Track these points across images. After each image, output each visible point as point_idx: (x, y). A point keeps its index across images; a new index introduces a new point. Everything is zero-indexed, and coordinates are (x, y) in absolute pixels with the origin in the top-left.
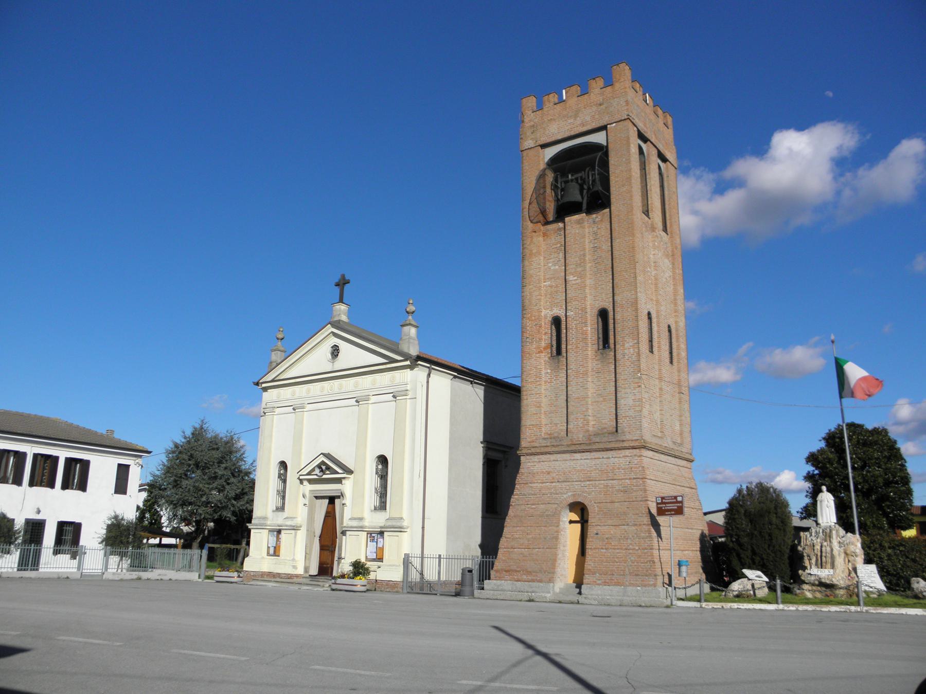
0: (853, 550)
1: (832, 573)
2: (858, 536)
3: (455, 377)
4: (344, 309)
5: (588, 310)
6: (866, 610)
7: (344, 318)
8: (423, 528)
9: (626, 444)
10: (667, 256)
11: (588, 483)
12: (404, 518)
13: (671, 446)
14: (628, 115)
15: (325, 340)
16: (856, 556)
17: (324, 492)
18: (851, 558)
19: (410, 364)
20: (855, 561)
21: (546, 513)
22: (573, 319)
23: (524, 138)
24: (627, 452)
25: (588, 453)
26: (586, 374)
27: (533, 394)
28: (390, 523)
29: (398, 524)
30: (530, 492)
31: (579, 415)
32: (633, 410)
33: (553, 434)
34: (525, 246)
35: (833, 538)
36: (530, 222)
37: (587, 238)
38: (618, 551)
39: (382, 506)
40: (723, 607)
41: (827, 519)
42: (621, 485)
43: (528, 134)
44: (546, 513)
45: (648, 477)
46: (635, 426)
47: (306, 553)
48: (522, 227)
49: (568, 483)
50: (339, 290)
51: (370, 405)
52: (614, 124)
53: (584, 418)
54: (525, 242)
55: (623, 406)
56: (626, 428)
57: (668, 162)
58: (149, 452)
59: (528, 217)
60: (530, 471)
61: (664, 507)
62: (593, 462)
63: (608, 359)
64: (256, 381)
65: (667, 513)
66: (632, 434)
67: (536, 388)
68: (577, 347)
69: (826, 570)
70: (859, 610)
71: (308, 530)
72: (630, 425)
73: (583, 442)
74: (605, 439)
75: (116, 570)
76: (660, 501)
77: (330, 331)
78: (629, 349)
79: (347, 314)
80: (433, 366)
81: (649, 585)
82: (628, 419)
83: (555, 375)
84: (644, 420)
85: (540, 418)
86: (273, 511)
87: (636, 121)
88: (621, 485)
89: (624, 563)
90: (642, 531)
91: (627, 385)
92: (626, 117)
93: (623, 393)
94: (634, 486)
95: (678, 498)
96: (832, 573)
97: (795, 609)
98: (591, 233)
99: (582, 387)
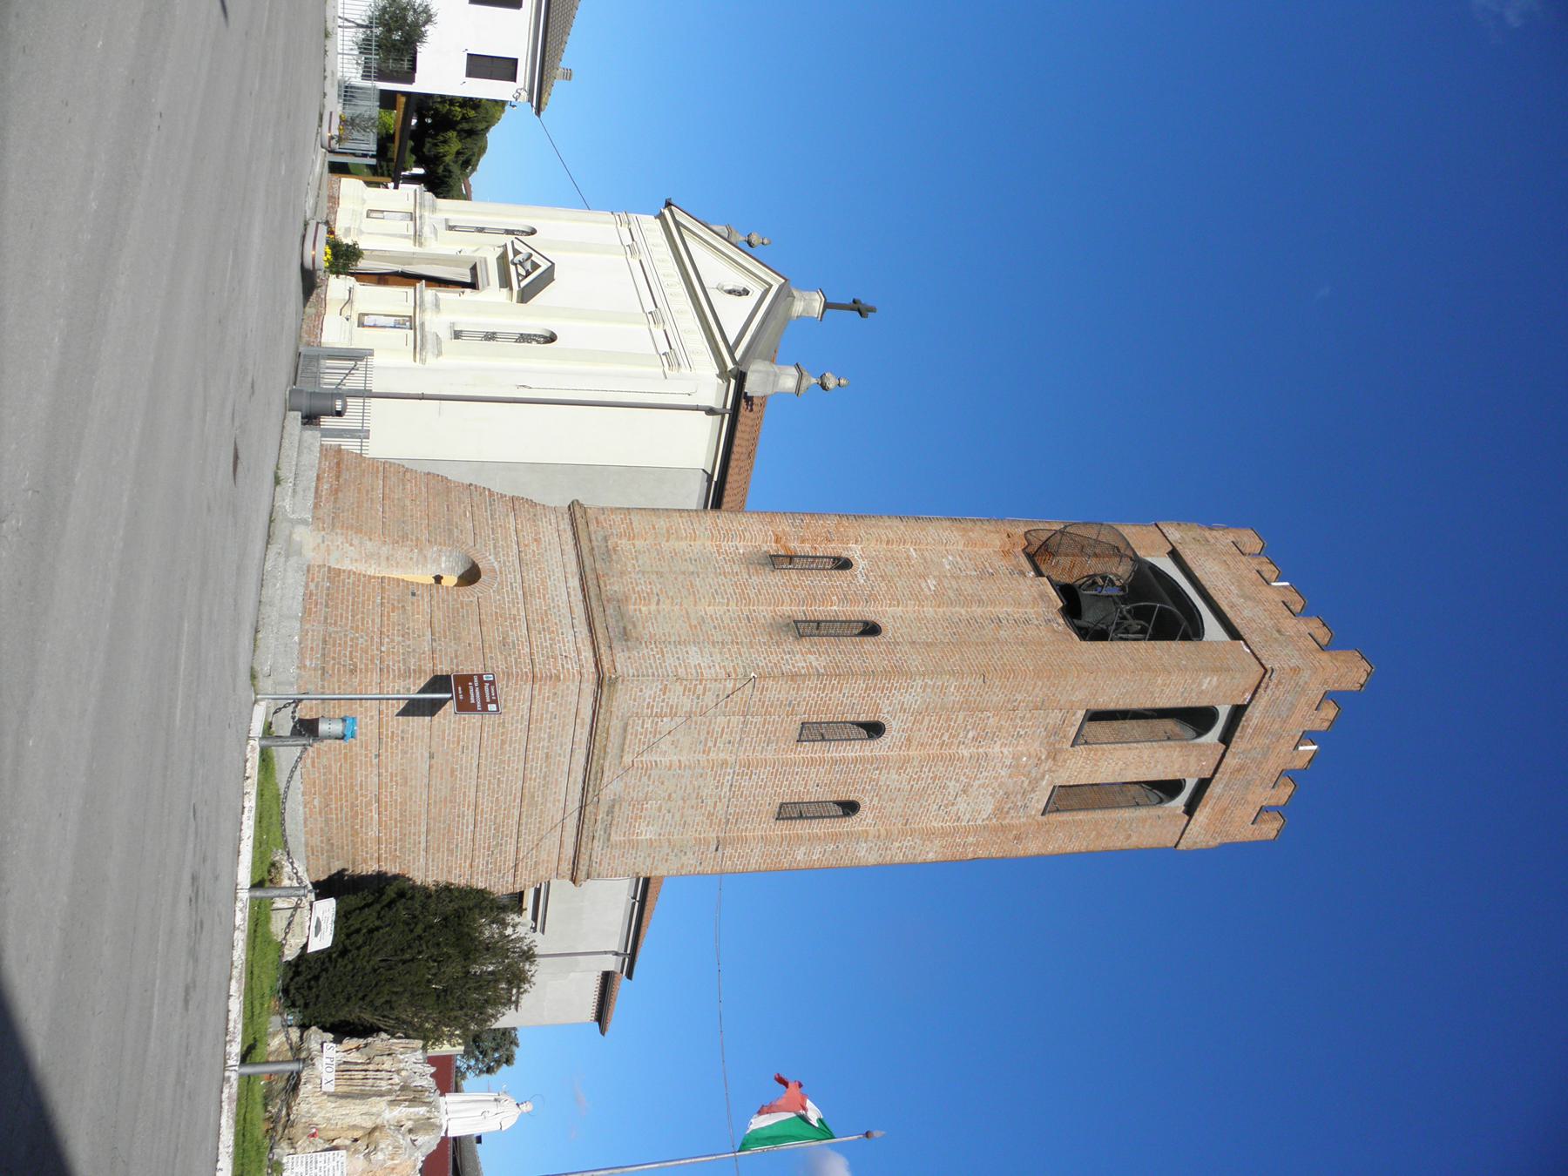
0: (382, 1146)
3: (710, 477)
4: (814, 307)
6: (229, 1077)
7: (798, 308)
8: (422, 397)
9: (603, 649)
11: (520, 593)
12: (440, 358)
13: (607, 794)
14: (1273, 670)
15: (759, 281)
16: (367, 1156)
17: (484, 272)
18: (361, 1145)
19: (729, 369)
20: (356, 1151)
21: (455, 530)
22: (851, 583)
23: (1181, 528)
24: (587, 654)
25: (581, 598)
27: (692, 524)
28: (430, 339)
29: (429, 346)
30: (497, 513)
31: (659, 586)
32: (677, 664)
33: (615, 554)
34: (979, 523)
35: (408, 1107)
36: (1026, 530)
37: (1016, 610)
38: (378, 620)
40: (248, 778)
41: (454, 1112)
42: (518, 640)
43: (1190, 533)
44: (455, 530)
45: (537, 686)
46: (644, 667)
47: (373, 250)
48: (1013, 521)
49: (517, 566)
50: (847, 303)
51: (647, 326)
52: (1249, 651)
53: (653, 594)
54: (987, 523)
56: (638, 653)
57: (1187, 817)
58: (538, 111)
59: (1035, 528)
60: (539, 517)
61: (473, 685)
62: (564, 605)
63: (779, 633)
64: (673, 201)
65: (460, 688)
66: (626, 662)
67: (706, 529)
69: (332, 1076)
70: (230, 1062)
71: (414, 253)
72: (644, 659)
73: (603, 590)
74: (612, 622)
75: (341, 15)
76: (485, 679)
77: (772, 282)
79: (805, 314)
80: (727, 416)
81: (302, 660)
82: (657, 656)
83: (735, 559)
87: (1263, 699)
88: (518, 640)
89: (352, 627)
90: (420, 660)
92: (1268, 666)
93: (712, 649)
94: (516, 659)
95: (495, 705)
97: (237, 924)
98: (1026, 616)
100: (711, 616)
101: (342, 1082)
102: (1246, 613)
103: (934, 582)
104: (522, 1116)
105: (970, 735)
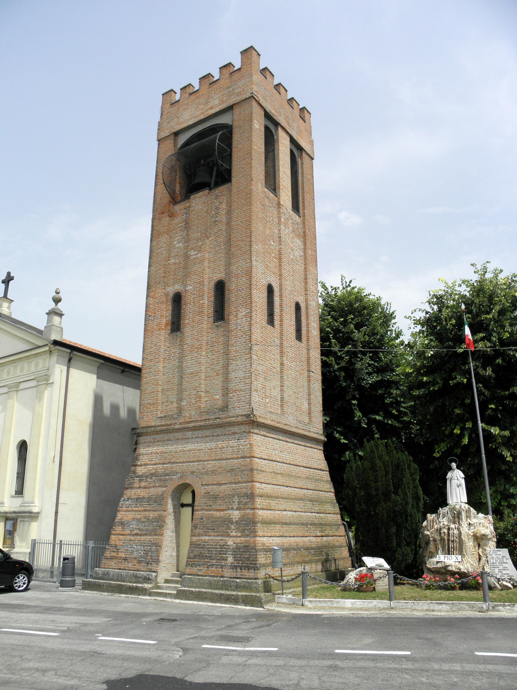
1: (460, 560)
2: (490, 517)
5: (206, 283)
8: (56, 513)
10: (298, 236)
26: (200, 348)
32: (243, 383)
39: (20, 492)
45: (256, 455)
50: (4, 286)
55: (234, 379)
68: (193, 320)
69: (454, 557)
78: (241, 319)
82: (238, 393)
84: (254, 394)
85: (157, 396)
86: (12, 497)
91: (238, 357)
92: (250, 95)
96: (460, 560)
99: (196, 361)
100: (210, 365)
101: (455, 552)
102: (216, 102)
103: (193, 251)
104: (458, 467)
105: (272, 243)
